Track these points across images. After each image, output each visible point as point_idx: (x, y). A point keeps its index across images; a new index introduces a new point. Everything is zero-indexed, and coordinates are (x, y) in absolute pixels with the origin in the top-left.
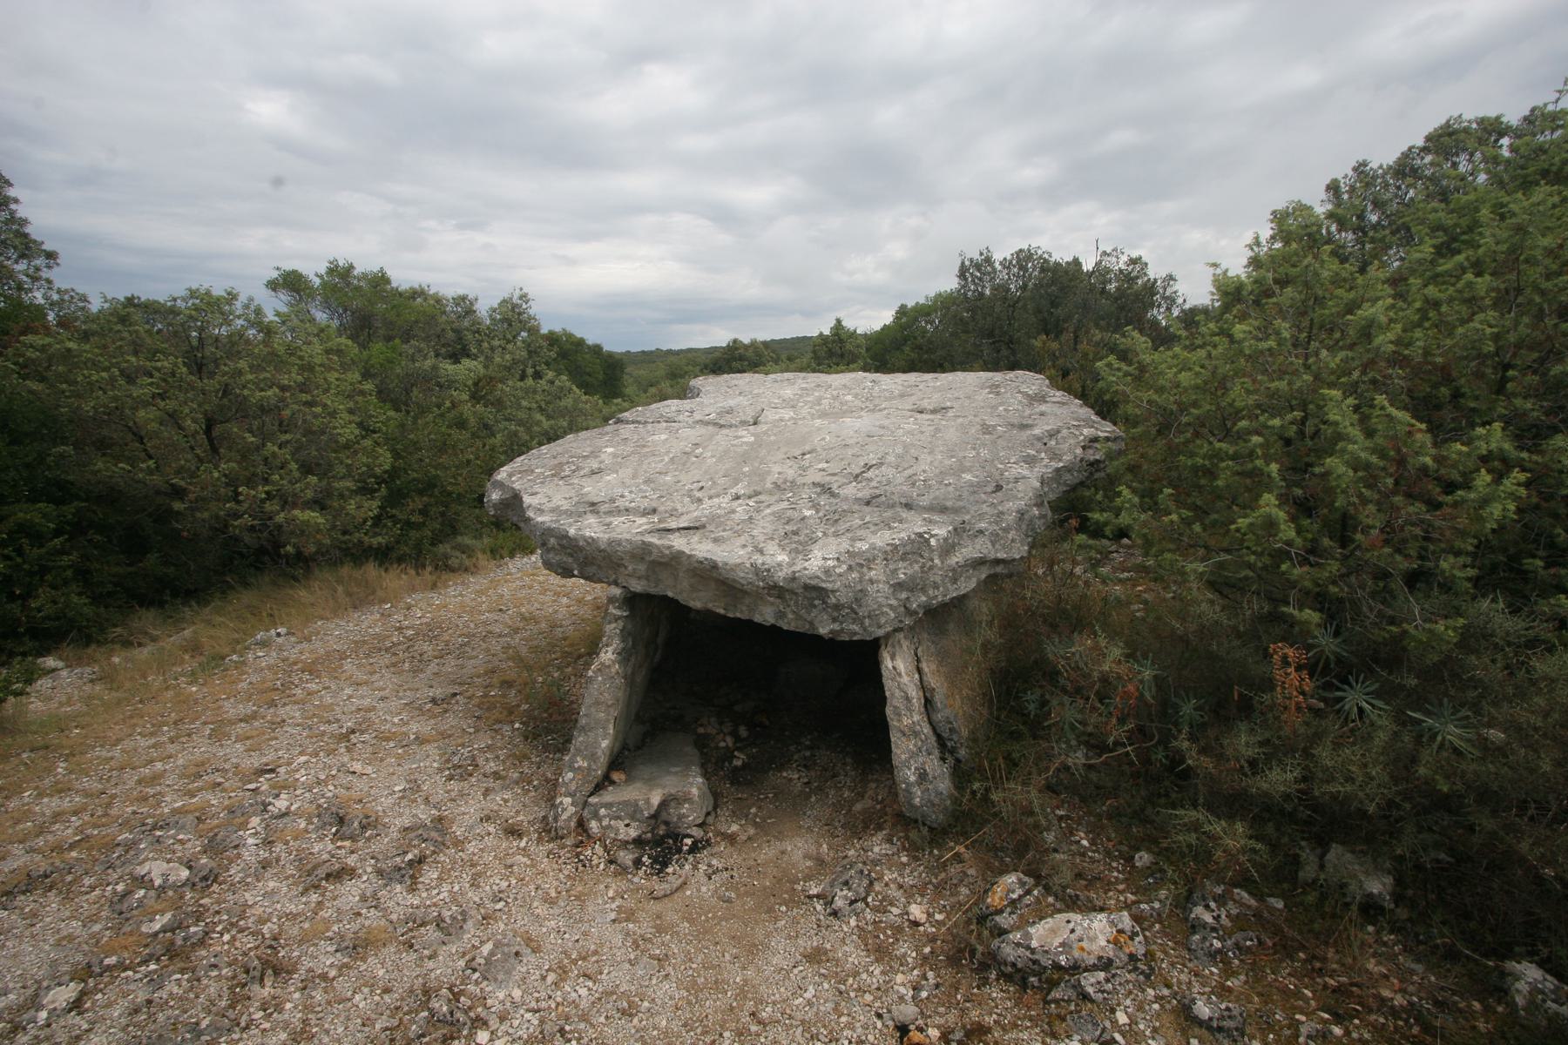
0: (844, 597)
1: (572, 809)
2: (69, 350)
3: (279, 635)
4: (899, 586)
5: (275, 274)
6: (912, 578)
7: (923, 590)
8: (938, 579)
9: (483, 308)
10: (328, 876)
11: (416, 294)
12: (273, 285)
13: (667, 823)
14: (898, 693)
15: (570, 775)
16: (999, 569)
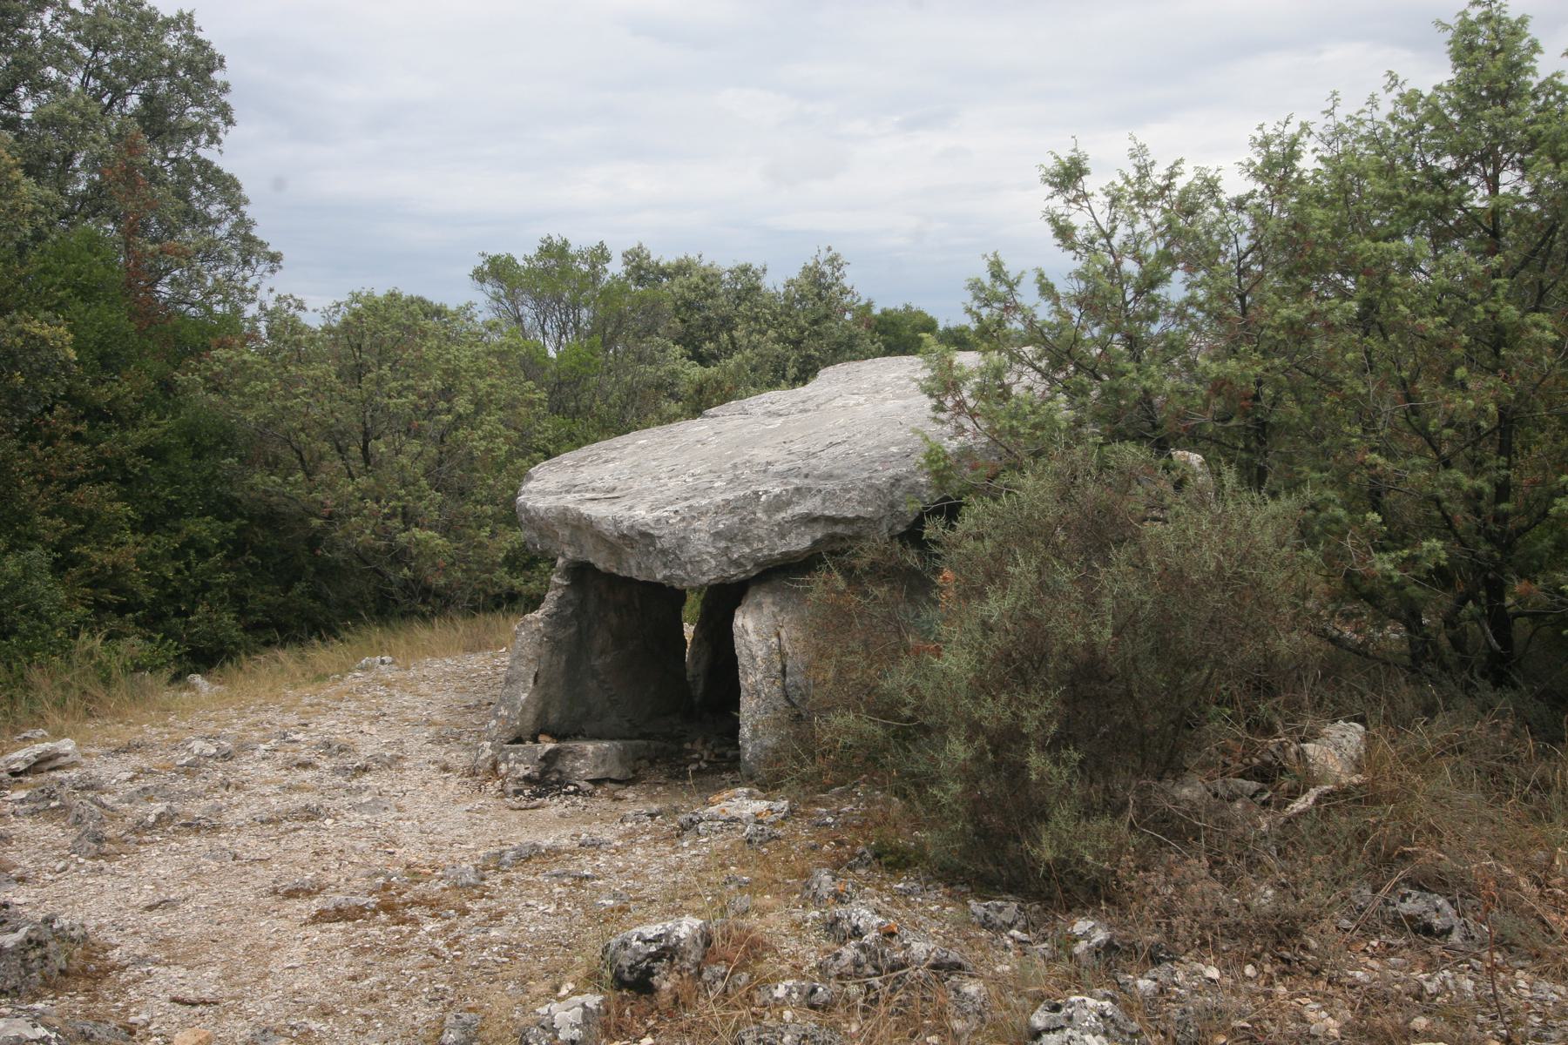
0: (665, 543)
1: (489, 752)
2: (245, 362)
3: (383, 662)
4: (718, 535)
5: (479, 262)
6: (729, 528)
7: (746, 541)
8: (762, 532)
9: (774, 282)
10: (298, 765)
11: (682, 269)
12: (479, 276)
13: (560, 772)
14: (745, 652)
15: (494, 722)
16: (839, 529)
